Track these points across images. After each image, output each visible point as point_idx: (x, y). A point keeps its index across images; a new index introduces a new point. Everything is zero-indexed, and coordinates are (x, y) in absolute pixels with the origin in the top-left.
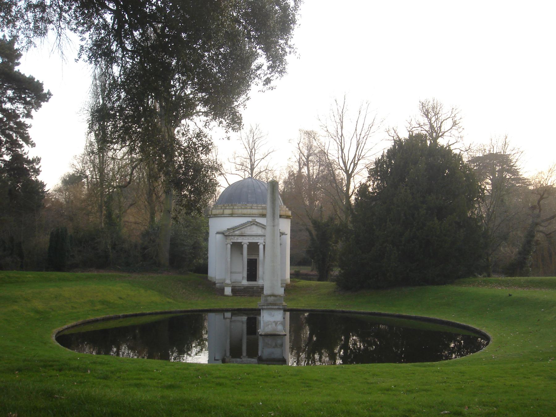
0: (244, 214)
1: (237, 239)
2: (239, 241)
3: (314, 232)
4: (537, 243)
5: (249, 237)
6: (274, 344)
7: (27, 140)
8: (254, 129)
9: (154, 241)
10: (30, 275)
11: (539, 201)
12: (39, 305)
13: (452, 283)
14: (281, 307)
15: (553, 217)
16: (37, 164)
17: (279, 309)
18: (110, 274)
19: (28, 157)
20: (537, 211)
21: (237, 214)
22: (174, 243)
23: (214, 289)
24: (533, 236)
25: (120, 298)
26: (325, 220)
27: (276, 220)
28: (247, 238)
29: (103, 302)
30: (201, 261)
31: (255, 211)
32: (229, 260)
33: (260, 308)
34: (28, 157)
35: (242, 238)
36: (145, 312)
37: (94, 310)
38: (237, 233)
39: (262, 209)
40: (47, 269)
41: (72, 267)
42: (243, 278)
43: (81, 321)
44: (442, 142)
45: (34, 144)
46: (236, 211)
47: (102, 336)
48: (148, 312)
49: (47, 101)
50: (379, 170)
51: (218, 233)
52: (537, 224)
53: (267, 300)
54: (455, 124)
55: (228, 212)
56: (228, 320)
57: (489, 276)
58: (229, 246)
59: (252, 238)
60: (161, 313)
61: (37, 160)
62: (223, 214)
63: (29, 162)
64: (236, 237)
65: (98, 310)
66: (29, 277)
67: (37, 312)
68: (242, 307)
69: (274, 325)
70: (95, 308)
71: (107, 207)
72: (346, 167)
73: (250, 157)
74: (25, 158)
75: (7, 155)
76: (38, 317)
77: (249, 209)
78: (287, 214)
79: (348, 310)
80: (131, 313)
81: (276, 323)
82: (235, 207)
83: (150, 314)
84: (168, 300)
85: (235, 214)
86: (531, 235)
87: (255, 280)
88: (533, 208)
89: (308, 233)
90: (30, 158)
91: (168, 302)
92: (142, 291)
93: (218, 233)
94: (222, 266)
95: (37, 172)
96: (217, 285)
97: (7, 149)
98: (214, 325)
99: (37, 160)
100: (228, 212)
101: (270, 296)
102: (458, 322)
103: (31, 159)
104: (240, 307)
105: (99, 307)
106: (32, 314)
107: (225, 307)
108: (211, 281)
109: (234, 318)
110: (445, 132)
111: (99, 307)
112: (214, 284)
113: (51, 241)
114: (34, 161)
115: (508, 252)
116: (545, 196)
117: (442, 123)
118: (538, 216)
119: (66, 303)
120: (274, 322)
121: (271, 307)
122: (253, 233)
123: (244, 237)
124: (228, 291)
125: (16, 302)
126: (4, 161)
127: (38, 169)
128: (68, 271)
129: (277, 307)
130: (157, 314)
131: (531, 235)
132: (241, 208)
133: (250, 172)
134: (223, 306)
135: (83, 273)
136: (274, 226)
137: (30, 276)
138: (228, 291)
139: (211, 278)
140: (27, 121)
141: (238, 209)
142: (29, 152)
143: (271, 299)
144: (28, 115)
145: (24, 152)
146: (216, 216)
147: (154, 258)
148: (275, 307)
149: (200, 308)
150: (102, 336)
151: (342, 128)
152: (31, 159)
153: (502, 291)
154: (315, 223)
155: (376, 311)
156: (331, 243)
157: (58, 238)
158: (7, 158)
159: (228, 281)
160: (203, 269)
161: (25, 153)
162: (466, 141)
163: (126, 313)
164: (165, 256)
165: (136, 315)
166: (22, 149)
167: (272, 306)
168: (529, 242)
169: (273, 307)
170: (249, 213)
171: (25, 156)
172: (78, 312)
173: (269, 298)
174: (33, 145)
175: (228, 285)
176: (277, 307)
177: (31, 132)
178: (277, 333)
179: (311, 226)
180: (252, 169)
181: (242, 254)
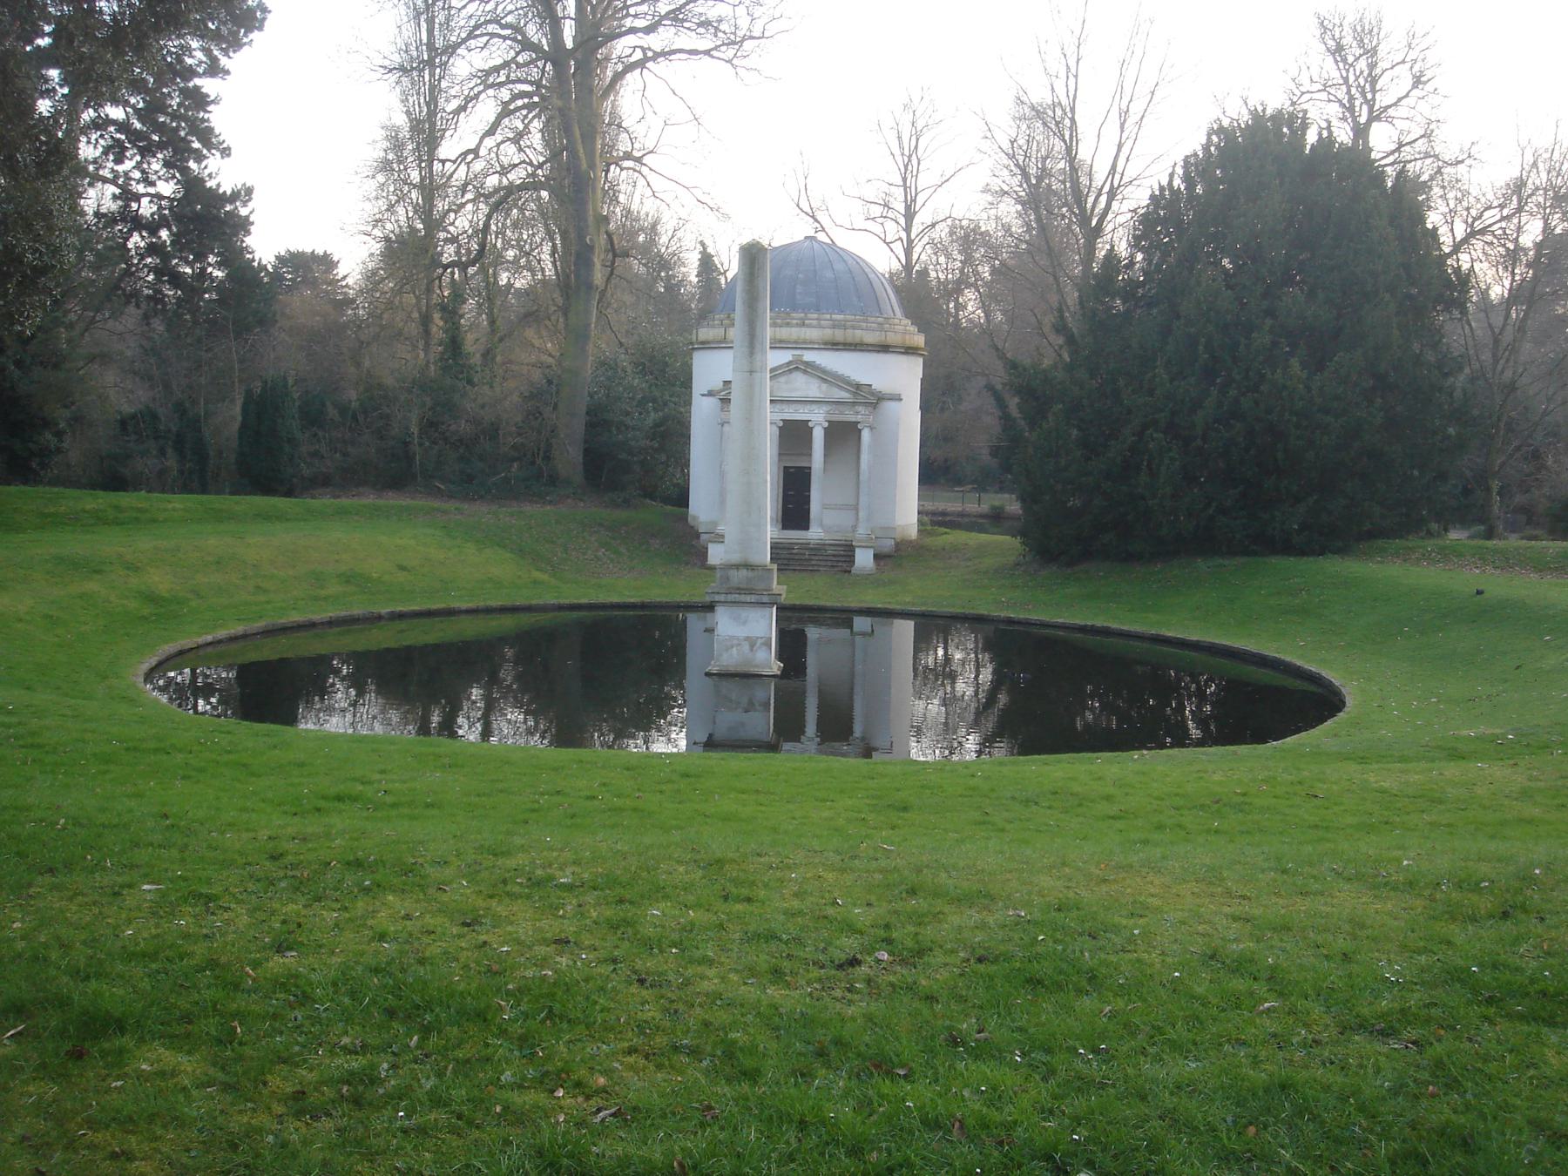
0: (781, 341)
5: (784, 406)
6: (745, 700)
7: (207, 135)
8: (916, 99)
12: (161, 581)
13: (1343, 551)
16: (245, 204)
19: (219, 185)
22: (597, 421)
25: (402, 568)
27: (758, 357)
29: (347, 578)
31: (812, 334)
33: (708, 599)
34: (219, 185)
36: (456, 604)
37: (317, 599)
39: (834, 327)
41: (320, 483)
43: (260, 624)
45: (229, 148)
48: (464, 605)
49: (260, 28)
50: (1160, 218)
51: (710, 394)
54: (1418, 81)
57: (1490, 534)
59: (793, 407)
60: (503, 610)
62: (724, 340)
63: (225, 199)
67: (152, 598)
69: (746, 647)
70: (323, 593)
73: (904, 180)
75: (167, 180)
76: (146, 612)
77: (797, 325)
78: (908, 343)
79: (1022, 616)
81: (752, 642)
83: (469, 612)
84: (537, 575)
87: (807, 528)
89: (992, 400)
90: (226, 188)
93: (710, 394)
97: (167, 164)
105: (334, 589)
106: (133, 605)
111: (334, 589)
114: (234, 197)
119: (244, 578)
120: (747, 639)
122: (796, 395)
124: (864, 559)
128: (289, 493)
129: (753, 598)
130: (488, 611)
133: (902, 221)
136: (751, 372)
137: (177, 506)
139: (695, 518)
140: (208, 85)
142: (221, 174)
143: (738, 577)
144: (214, 70)
145: (207, 172)
146: (706, 345)
148: (748, 598)
149: (615, 599)
153: (1462, 579)
155: (1099, 622)
158: (167, 188)
160: (682, 499)
161: (210, 175)
163: (399, 609)
164: (569, 457)
165: (429, 614)
167: (746, 593)
169: (743, 598)
170: (794, 337)
171: (210, 184)
173: (733, 573)
174: (226, 152)
176: (753, 598)
177: (217, 118)
180: (910, 215)
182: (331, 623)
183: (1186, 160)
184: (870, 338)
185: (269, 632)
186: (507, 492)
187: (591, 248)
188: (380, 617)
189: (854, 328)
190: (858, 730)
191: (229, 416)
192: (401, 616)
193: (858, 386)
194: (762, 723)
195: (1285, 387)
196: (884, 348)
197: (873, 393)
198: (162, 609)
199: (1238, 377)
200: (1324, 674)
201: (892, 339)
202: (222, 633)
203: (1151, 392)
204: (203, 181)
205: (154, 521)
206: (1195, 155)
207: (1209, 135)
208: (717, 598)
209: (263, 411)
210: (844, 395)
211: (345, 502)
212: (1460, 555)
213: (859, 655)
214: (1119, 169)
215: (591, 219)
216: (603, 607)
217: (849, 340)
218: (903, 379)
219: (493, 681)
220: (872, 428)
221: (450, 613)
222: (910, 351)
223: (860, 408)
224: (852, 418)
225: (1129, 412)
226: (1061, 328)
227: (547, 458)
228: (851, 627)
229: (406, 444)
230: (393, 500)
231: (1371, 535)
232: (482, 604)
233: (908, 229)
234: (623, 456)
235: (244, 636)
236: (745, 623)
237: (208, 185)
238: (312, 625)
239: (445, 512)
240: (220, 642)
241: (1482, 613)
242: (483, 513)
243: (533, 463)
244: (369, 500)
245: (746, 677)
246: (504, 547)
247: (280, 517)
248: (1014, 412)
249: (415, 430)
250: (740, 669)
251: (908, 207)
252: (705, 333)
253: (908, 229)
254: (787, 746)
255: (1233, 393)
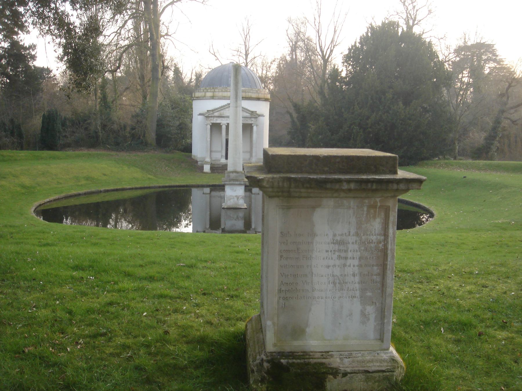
0: (224, 97)
1: (217, 120)
2: (218, 122)
3: (295, 115)
4: (504, 129)
6: (235, 217)
9: (141, 122)
10: (23, 154)
11: (508, 89)
12: (26, 181)
14: (242, 183)
15: (518, 106)
16: (33, 50)
17: (240, 184)
18: (99, 152)
20: (505, 99)
21: (217, 97)
22: (160, 124)
23: (195, 166)
24: (499, 123)
25: (105, 175)
26: (306, 104)
28: (226, 119)
29: (87, 178)
30: (188, 141)
32: (209, 140)
33: (223, 183)
35: (221, 119)
36: (125, 187)
37: (78, 186)
38: (216, 114)
40: (41, 149)
41: (66, 146)
42: (222, 156)
43: (63, 195)
44: (416, 30)
46: (217, 94)
47: (98, 210)
48: (128, 187)
50: (353, 56)
51: (200, 114)
52: (503, 112)
53: (229, 176)
54: (430, 12)
55: (209, 94)
56: (208, 196)
58: (209, 127)
60: (141, 188)
61: (33, 47)
63: (26, 49)
64: (215, 119)
65: (81, 185)
66: (22, 156)
67: (23, 187)
68: (217, 183)
69: (236, 199)
70: (80, 184)
71: (101, 90)
72: (322, 52)
73: (245, 43)
74: (21, 45)
76: (23, 191)
80: (112, 188)
81: (238, 197)
82: (216, 90)
83: (130, 189)
85: (216, 97)
86: (497, 122)
88: (502, 95)
90: (27, 45)
91: (149, 179)
92: (126, 168)
93: (200, 114)
94: (200, 147)
95: (33, 58)
96: (199, 163)
98: (198, 198)
99: (33, 47)
100: (209, 94)
101: (233, 172)
102: (411, 201)
103: (28, 46)
104: (214, 183)
105: (83, 182)
106: (19, 189)
107: (204, 183)
108: (194, 159)
109: (214, 193)
110: (420, 21)
111: (83, 182)
112: (197, 162)
113: (43, 122)
115: (478, 137)
116: (513, 84)
117: (417, 11)
118: (505, 104)
120: (236, 196)
121: (232, 182)
123: (223, 119)
124: (207, 168)
125: (5, 178)
126: (3, 48)
127: (34, 55)
129: (238, 183)
130: (136, 189)
131: (497, 122)
132: (222, 91)
134: (204, 182)
135: (73, 152)
136: (236, 107)
137: (23, 154)
138: (207, 168)
141: (219, 92)
143: (233, 175)
145: (20, 39)
146: (198, 98)
147: (141, 137)
148: (237, 183)
149: (177, 184)
150: (98, 210)
151: (319, 17)
152: (28, 46)
154: (296, 107)
156: (310, 125)
157: (50, 121)
159: (208, 159)
160: (188, 149)
161: (21, 40)
162: (444, 36)
163: (107, 188)
164: (151, 136)
165: (117, 190)
166: (19, 36)
167: (234, 182)
168: (494, 129)
171: (21, 43)
172: (63, 187)
175: (207, 163)
176: (238, 183)
178: (238, 207)
179: (292, 110)
180: (247, 55)
181: (221, 133)
182: (85, 194)
183: (361, 38)
184: (254, 96)
185: (66, 197)
186: (131, 148)
187: (158, 66)
188: (101, 192)
189: (249, 92)
190: (253, 227)
191: (37, 122)
192: (107, 191)
193: (252, 112)
194: (240, 224)
195: (398, 112)
196: (258, 99)
197: (257, 114)
198: (29, 191)
199: (382, 108)
200: (47, 222)
201: (261, 96)
202: (52, 198)
203: (353, 113)
204: (18, 42)
205: (16, 160)
206: (363, 35)
207: (368, 29)
208: (226, 183)
209: (50, 121)
210: (248, 115)
211: (77, 152)
212: (452, 165)
213: (253, 201)
214: (335, 40)
215: (157, 56)
216: (174, 186)
217: (247, 96)
218: (264, 109)
219: (117, 213)
220: (257, 125)
221: (123, 190)
222: (266, 100)
223: (253, 119)
224: (250, 122)
225: (346, 120)
226: (321, 93)
227: (144, 136)
228: (251, 192)
229: (96, 132)
230: (93, 152)
231: (423, 159)
232: (133, 186)
233: (246, 59)
234: (169, 136)
235: (58, 199)
236: (235, 191)
237: (21, 43)
238: (79, 195)
239: (112, 155)
240: (51, 201)
241: (467, 183)
242: (124, 155)
243: (140, 138)
244: (85, 152)
245: (236, 209)
246: (137, 167)
247: (59, 158)
248: (296, 120)
249: (99, 128)
250: (234, 206)
251: (246, 52)
252: (197, 94)
253: (246, 59)
254: (248, 232)
255: (380, 113)
